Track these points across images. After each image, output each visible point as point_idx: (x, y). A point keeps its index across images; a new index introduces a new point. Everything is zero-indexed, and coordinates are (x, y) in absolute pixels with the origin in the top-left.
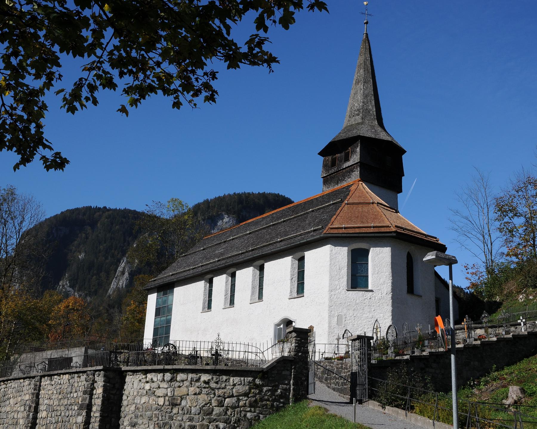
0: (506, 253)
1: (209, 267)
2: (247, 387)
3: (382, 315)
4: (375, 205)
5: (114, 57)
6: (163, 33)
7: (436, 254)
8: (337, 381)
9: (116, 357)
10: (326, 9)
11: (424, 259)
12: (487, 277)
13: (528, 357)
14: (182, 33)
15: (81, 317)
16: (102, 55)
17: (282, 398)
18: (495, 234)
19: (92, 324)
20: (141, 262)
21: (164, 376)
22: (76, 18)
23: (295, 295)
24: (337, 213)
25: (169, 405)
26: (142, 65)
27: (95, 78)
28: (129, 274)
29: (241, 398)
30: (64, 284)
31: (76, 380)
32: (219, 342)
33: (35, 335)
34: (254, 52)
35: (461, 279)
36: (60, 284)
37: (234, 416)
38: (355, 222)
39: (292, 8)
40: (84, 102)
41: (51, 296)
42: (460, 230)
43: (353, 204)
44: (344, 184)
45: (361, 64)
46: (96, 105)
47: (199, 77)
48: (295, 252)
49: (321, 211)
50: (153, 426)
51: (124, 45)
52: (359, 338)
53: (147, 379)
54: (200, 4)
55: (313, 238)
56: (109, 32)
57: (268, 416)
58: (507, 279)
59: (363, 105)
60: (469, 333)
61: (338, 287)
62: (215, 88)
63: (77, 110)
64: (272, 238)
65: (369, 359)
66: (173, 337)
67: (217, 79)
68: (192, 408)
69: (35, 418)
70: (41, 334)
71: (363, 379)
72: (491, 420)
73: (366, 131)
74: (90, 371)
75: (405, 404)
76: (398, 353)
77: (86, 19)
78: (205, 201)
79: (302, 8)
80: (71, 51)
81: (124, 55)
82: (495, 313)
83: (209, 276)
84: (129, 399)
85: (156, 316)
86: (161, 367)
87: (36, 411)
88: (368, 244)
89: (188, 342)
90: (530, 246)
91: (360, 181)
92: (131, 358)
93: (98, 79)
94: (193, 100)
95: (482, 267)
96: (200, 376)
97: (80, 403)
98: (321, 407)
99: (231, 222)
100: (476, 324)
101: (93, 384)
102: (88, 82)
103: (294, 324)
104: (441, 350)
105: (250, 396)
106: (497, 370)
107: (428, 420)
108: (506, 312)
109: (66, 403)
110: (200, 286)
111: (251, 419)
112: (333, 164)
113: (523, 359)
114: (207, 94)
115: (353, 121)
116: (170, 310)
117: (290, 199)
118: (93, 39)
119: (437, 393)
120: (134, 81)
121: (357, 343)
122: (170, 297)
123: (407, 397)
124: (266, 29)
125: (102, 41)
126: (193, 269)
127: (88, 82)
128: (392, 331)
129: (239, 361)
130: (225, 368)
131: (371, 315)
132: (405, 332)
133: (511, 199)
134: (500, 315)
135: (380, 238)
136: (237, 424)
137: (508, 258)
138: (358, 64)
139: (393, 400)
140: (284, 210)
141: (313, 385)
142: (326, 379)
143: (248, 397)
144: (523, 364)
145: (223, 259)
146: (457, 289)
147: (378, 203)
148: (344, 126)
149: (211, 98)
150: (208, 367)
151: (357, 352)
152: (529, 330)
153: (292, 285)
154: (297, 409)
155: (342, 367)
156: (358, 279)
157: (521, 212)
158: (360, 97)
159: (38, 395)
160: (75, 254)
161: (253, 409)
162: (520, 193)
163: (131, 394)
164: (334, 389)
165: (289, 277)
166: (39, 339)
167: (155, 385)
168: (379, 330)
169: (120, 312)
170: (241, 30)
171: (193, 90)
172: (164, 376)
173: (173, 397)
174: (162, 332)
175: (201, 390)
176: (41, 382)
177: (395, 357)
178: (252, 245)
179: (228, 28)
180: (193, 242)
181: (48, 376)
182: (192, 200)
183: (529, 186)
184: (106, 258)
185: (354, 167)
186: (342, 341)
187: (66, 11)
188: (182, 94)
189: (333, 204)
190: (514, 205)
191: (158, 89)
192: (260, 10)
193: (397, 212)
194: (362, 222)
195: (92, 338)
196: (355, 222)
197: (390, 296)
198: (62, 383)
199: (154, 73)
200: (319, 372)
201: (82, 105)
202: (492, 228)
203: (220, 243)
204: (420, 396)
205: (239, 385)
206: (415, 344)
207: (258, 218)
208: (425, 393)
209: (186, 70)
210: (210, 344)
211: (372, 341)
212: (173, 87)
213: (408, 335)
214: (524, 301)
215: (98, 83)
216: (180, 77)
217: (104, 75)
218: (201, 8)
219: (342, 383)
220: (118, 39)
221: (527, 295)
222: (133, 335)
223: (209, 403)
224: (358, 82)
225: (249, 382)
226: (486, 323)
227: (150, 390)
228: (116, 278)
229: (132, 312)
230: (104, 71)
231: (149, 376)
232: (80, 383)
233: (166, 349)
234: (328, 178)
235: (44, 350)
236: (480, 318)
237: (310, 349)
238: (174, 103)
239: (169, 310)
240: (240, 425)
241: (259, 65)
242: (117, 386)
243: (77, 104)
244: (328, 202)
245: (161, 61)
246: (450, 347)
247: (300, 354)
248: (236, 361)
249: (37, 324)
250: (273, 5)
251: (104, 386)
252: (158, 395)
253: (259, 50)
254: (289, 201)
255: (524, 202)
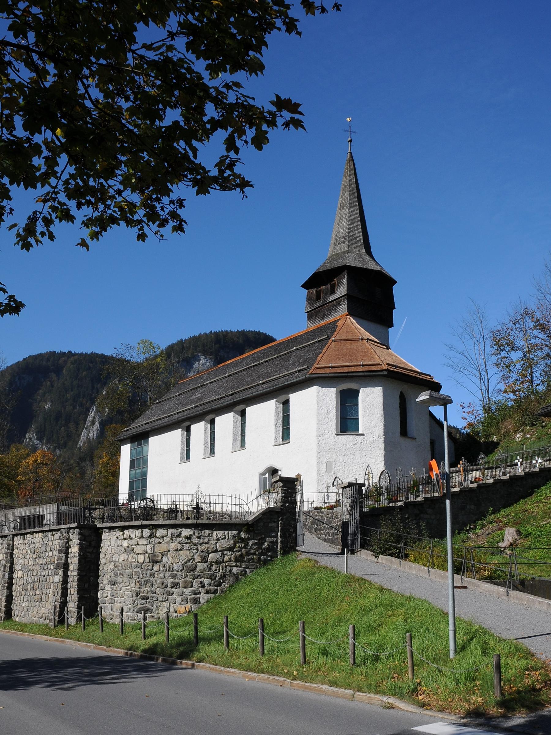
0: (503, 390)
1: (186, 413)
2: (232, 542)
3: (374, 460)
4: (365, 341)
5: (70, 186)
6: (124, 158)
7: (430, 394)
8: (328, 531)
9: (90, 514)
10: (303, 127)
11: (417, 400)
12: (483, 415)
13: (524, 499)
14: (145, 157)
15: (51, 471)
16: (57, 185)
17: (269, 552)
18: (492, 370)
19: (64, 479)
20: (111, 410)
21: (142, 532)
22: (26, 145)
23: (280, 441)
24: (324, 351)
25: (150, 562)
26: (102, 195)
27: (50, 210)
28: (100, 424)
29: (225, 552)
30: (31, 437)
31: (50, 539)
32: (199, 494)
33: (4, 492)
34: (225, 175)
35: (457, 418)
36: (27, 436)
37: (219, 571)
38: (343, 360)
39: (265, 127)
40: (39, 237)
41: (18, 450)
42: (455, 367)
43: (341, 340)
44: (331, 319)
45: (345, 186)
46: (53, 240)
47: (164, 205)
48: (280, 395)
49: (306, 349)
50: (134, 584)
51: (80, 173)
52: (350, 485)
53: (125, 536)
54: (162, 125)
55: (298, 379)
56: (63, 159)
57: (255, 571)
58: (504, 418)
59: (349, 232)
60: (465, 476)
61: (326, 432)
62: (183, 217)
63: (32, 247)
64: (253, 381)
65: (361, 507)
66: (151, 491)
67: (184, 207)
68: (174, 564)
69: (11, 578)
70: (10, 490)
71: (355, 528)
72: (486, 564)
73: (353, 261)
74: (64, 529)
75: (399, 552)
76: (392, 499)
77: (38, 146)
78: (178, 342)
79: (276, 126)
80: (22, 183)
81: (81, 183)
82: (491, 453)
83: (186, 424)
84: (107, 557)
85: (131, 468)
86: (138, 523)
87: (12, 571)
88: (358, 385)
89: (166, 496)
90: (528, 382)
91: (347, 315)
92: (106, 514)
93: (53, 211)
94: (159, 231)
95: (479, 405)
96: (181, 531)
97: (56, 562)
98: (312, 559)
99: (208, 364)
100: (472, 466)
101: (67, 542)
102: (42, 215)
103: (279, 473)
104: (436, 494)
105: (235, 550)
106: (493, 513)
107: (423, 567)
108: (503, 453)
109: (41, 562)
110: (177, 434)
111: (237, 574)
112: (318, 297)
113: (519, 500)
114: (175, 224)
115: (338, 250)
116: (145, 462)
117: (272, 337)
118: (46, 167)
119: (432, 540)
120: (94, 212)
121: (348, 491)
122: (145, 448)
123: (401, 545)
124: (237, 151)
125: (56, 169)
126: (169, 416)
127: (42, 215)
128: (385, 476)
129: (222, 514)
130: (207, 522)
131: (362, 460)
132: (398, 477)
133: (508, 332)
134: (497, 455)
135: (371, 377)
136: (223, 579)
137: (506, 395)
138: (342, 186)
139: (387, 549)
140: (265, 349)
141: (302, 536)
142: (316, 530)
143: (234, 552)
144: (519, 506)
145: (201, 405)
146: (453, 430)
147: (368, 339)
148: (329, 255)
149: (179, 228)
150: (189, 522)
151: (348, 500)
152: (526, 470)
153: (276, 430)
154: (286, 562)
155: (332, 516)
156: (347, 423)
157: (518, 346)
158: (345, 223)
159: (12, 555)
160: (40, 404)
161: (238, 564)
162: (517, 326)
163: (109, 551)
164: (324, 540)
165: (273, 423)
166: (9, 496)
167: (133, 542)
168: (370, 476)
169: (92, 465)
170: (209, 153)
171: (159, 219)
172: (142, 532)
173: (153, 554)
174: (138, 486)
175: (183, 545)
176: (13, 541)
177: (388, 504)
178: (232, 388)
179: (195, 151)
180: (167, 387)
181: (21, 534)
182: (164, 340)
183: (527, 318)
184: (74, 407)
185: (341, 300)
186: (332, 489)
187: (13, 138)
188: (148, 225)
189: (319, 341)
190: (511, 338)
191: (120, 219)
192: (230, 130)
193: (388, 348)
194: (351, 360)
195: (64, 494)
196: (343, 360)
197: (383, 439)
198: (35, 542)
199: (115, 202)
200: (308, 523)
201: (37, 241)
202: (489, 363)
203: (196, 388)
204: (415, 543)
205: (223, 539)
206: (410, 490)
207: (237, 358)
208: (419, 540)
209: (151, 198)
210: (190, 496)
211: (363, 488)
212: (136, 217)
213: (402, 480)
214: (521, 440)
215: (54, 215)
216: (144, 206)
217: (60, 207)
218: (163, 130)
219: (333, 533)
220: (74, 167)
221: (524, 434)
222: (108, 490)
223: (191, 559)
224: (342, 206)
225: (234, 536)
226: (483, 464)
227: (128, 547)
228: (86, 428)
229: (105, 465)
230: (59, 203)
231: (127, 532)
232: (54, 542)
233: (143, 504)
234: (312, 313)
235: (14, 508)
236: (476, 459)
237: (298, 498)
238: (139, 235)
239: (145, 462)
240: (226, 580)
241: (231, 189)
242: (93, 543)
243: (31, 240)
244: (314, 339)
245: (122, 189)
246: (445, 491)
247: (287, 505)
248: (219, 513)
249: (6, 480)
250: (244, 124)
251: (80, 544)
252: (137, 552)
253: (230, 173)
254: (272, 339)
255: (522, 335)
